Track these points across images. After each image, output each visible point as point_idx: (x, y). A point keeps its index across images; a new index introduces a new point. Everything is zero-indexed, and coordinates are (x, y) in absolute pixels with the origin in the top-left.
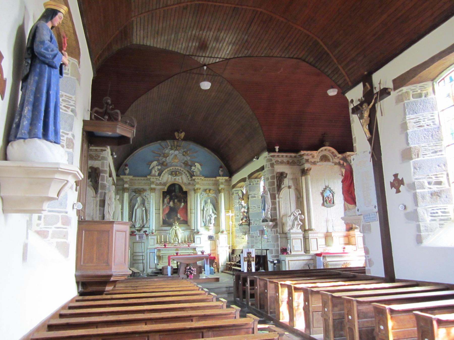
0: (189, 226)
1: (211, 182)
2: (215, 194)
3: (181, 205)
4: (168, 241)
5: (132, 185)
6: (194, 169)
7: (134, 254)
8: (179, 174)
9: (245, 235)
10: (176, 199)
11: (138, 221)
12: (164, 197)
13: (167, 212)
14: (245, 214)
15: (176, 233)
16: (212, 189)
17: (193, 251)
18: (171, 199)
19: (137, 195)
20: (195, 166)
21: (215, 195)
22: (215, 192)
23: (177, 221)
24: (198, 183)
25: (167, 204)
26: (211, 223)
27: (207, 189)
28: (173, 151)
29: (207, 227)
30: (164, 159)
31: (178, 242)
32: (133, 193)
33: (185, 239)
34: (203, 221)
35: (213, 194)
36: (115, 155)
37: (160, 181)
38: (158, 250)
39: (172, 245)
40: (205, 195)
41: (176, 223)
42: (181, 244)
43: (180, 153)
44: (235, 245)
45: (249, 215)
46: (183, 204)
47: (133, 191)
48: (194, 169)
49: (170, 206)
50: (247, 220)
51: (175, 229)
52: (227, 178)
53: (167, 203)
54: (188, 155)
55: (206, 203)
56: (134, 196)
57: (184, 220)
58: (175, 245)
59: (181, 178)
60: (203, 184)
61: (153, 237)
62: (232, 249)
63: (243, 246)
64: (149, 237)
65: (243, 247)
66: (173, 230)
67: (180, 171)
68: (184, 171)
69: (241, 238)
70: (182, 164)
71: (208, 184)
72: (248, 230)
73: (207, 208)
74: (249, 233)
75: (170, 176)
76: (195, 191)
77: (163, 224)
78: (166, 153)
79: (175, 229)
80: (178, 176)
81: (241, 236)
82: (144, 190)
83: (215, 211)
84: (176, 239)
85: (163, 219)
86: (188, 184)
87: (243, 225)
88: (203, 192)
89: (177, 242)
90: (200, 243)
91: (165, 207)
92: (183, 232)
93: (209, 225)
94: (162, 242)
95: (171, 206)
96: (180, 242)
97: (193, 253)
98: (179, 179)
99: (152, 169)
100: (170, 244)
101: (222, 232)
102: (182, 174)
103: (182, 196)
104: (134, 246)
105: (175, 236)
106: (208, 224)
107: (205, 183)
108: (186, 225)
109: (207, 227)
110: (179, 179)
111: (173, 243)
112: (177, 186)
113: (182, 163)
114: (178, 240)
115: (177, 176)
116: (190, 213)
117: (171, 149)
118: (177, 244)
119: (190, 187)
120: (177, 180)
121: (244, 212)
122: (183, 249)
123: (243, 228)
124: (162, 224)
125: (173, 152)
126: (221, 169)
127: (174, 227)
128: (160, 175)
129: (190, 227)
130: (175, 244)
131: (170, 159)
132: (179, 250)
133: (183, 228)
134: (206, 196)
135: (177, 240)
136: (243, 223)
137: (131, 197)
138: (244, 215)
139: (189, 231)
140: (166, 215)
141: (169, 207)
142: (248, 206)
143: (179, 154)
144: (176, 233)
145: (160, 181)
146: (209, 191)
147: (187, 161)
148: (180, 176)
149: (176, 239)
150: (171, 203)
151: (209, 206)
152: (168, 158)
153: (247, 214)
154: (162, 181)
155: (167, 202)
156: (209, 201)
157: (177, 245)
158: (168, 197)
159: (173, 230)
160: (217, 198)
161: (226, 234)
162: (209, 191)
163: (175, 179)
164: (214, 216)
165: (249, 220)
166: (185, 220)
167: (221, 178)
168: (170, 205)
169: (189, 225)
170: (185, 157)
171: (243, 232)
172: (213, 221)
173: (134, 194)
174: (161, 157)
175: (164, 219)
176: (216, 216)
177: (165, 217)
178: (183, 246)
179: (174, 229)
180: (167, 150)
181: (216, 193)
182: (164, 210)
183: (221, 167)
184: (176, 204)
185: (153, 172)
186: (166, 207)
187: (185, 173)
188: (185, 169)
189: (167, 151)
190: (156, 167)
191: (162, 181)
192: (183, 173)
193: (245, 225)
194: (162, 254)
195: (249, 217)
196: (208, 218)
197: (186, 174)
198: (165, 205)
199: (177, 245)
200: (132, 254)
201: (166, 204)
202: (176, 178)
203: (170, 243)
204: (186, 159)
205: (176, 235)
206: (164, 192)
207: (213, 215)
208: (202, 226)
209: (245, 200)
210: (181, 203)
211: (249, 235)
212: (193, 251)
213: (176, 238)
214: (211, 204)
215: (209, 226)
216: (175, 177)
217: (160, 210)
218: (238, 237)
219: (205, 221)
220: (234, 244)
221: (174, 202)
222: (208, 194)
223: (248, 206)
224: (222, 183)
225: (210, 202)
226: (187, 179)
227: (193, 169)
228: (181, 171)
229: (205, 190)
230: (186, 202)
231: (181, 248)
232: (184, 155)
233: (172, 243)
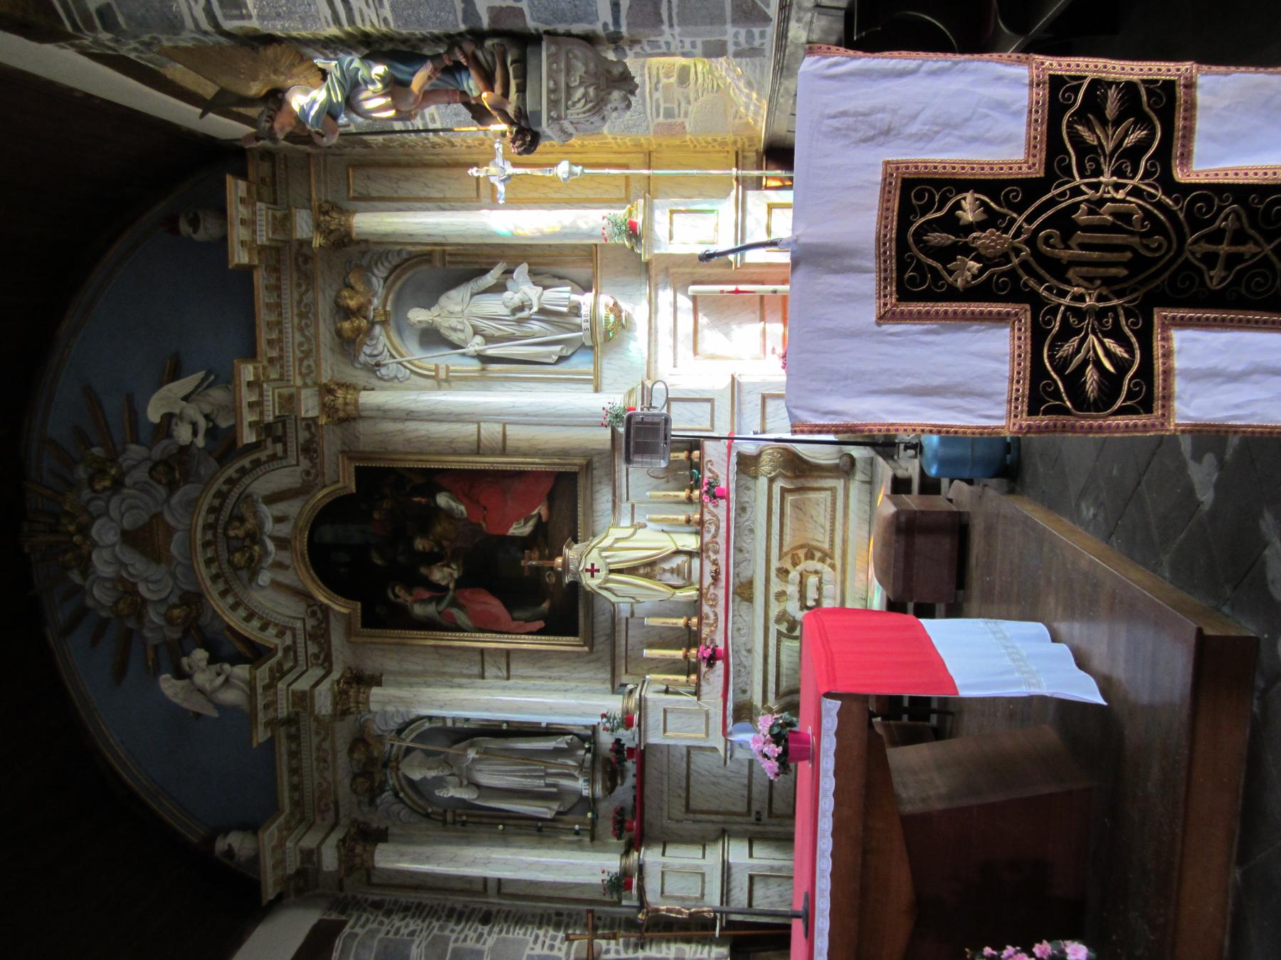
0: (588, 467)
1: (290, 296)
2: (369, 269)
3: (449, 514)
4: (681, 622)
5: (336, 803)
6: (194, 425)
7: (755, 807)
8: (242, 520)
9: (624, 81)
10: (410, 541)
11: (550, 780)
12: (403, 620)
13: (495, 606)
14: (420, 79)
15: (632, 571)
16: (338, 296)
17: (763, 482)
18: (415, 581)
19: (392, 781)
20: (168, 418)
21: (381, 272)
22: (359, 267)
23: (552, 557)
24: (290, 401)
25: (446, 602)
26: (575, 310)
27: (339, 333)
28: (94, 556)
29: (600, 338)
30: (154, 616)
31: (690, 554)
32: (378, 801)
33: (674, 661)
34: (561, 359)
35: (368, 283)
36: (582, 171)
37: (301, 640)
38: (738, 717)
39: (715, 599)
40: (382, 340)
41: (565, 564)
42: (707, 537)
43: (106, 513)
44: (730, 138)
45: (436, 39)
46: (442, 500)
47: (372, 802)
48: (194, 425)
49: (460, 584)
50: (474, 59)
51: (603, 573)
52: (236, 188)
53: (439, 601)
54: (113, 458)
55: (432, 337)
56: (396, 795)
57: (551, 499)
58: (716, 578)
59: (272, 499)
60: (307, 354)
61: (654, 717)
62: (759, 167)
63: (741, 84)
64: (653, 739)
65: (749, 84)
66: (607, 589)
67: (224, 516)
68: (219, 484)
69: (678, 92)
70: (175, 499)
71: (302, 316)
72: (579, 50)
73: (470, 330)
74: (615, 40)
75: (265, 578)
76: (348, 418)
77: (574, 633)
78: (116, 603)
79: (603, 573)
80: (261, 525)
81: (668, 87)
82: (361, 740)
83: (490, 279)
84: (676, 571)
85: (540, 632)
86: (311, 460)
87: (521, 112)
88: (362, 358)
89: (696, 562)
90: (707, 406)
91: (461, 617)
92: (625, 507)
93: (583, 321)
94: (687, 626)
95: (456, 575)
96: (691, 543)
97: (771, 480)
98: (279, 520)
99: (219, 706)
100: (706, 609)
101: (633, 232)
102: (246, 498)
103: (386, 504)
104: (705, 807)
105: (648, 576)
106: (579, 328)
107: (298, 338)
108: (581, 482)
109: (600, 338)
110: (279, 520)
111: (700, 590)
112: (328, 533)
113: (167, 500)
114: (678, 552)
115: (262, 533)
116: (504, 451)
117: (85, 565)
118: (709, 567)
119: (331, 443)
120: (284, 530)
121: (395, 87)
122: (739, 550)
123: (553, 104)
124: (572, 638)
125: (106, 554)
126: (184, 228)
127: (590, 582)
128: (255, 653)
129: (600, 453)
130: (708, 580)
131: (156, 571)
132: (746, 574)
133: (603, 500)
134: (383, 340)
135: (679, 560)
136: (511, 110)
137: (404, 813)
138: (429, 95)
139: (621, 467)
140: (516, 615)
141: (467, 593)
142: (330, 45)
143: (114, 513)
144: (632, 571)
145: (301, 640)
146: (348, 313)
147: (156, 464)
148: (264, 508)
149: (672, 571)
150: (439, 575)
151: (453, 322)
152: (142, 589)
153: (422, 59)
154: (299, 624)
155: (430, 601)
156: (418, 315)
157: (715, 563)
158: (401, 594)
159: (607, 589)
160: (395, 261)
161: (649, 210)
162: (348, 313)
163: (282, 543)
164: (524, 290)
165: (477, 36)
166: (546, 485)
167: (238, 234)
168: (452, 586)
169: (584, 462)
170: (128, 481)
171: (598, 107)
172: (560, 296)
173: (387, 795)
174: (148, 634)
175: (540, 624)
176: (522, 271)
177: (527, 620)
178: (723, 525)
179: (607, 581)
180: (96, 592)
181: (365, 262)
182: (485, 626)
183: (171, 224)
184: (445, 543)
185: (231, 696)
186: (461, 607)
187: (230, 481)
188: (213, 478)
189: (101, 595)
190: (201, 679)
191: (299, 624)
192: (236, 491)
193: (522, 89)
194: (771, 696)
195: (453, 40)
196: (536, 326)
197: (243, 472)
198: (451, 616)
199: (715, 563)
200: (758, 819)
201: (443, 606)
202: (274, 538)
203: (695, 607)
204: (141, 474)
205: (648, 568)
206: (372, 620)
207: (512, 297)
208: (591, 368)
209: (278, 80)
210: (438, 508)
211: (634, 42)
212: (763, 482)
213: (667, 566)
214: (443, 300)
215: (593, 320)
216: (271, 546)
217: (482, 651)
218: (669, 114)
219: (557, 348)
220: (723, 144)
221: (432, 559)
222: (372, 324)
223: (330, 45)
224: (283, 223)
225: (428, 306)
226: (275, 464)
227: (195, 434)
228: (222, 505)
229: (348, 345)
230: (433, 479)
231: (736, 565)
232: (118, 484)
233: (701, 595)
